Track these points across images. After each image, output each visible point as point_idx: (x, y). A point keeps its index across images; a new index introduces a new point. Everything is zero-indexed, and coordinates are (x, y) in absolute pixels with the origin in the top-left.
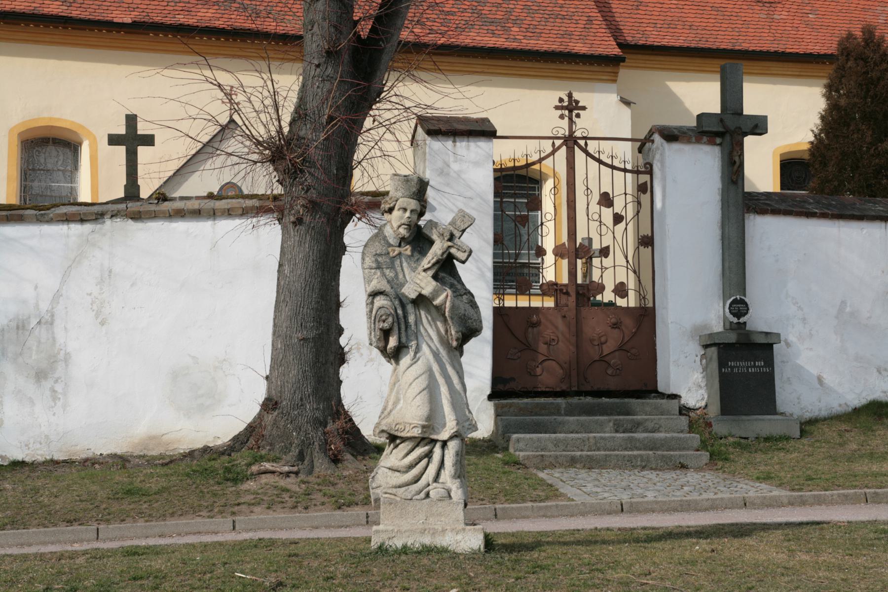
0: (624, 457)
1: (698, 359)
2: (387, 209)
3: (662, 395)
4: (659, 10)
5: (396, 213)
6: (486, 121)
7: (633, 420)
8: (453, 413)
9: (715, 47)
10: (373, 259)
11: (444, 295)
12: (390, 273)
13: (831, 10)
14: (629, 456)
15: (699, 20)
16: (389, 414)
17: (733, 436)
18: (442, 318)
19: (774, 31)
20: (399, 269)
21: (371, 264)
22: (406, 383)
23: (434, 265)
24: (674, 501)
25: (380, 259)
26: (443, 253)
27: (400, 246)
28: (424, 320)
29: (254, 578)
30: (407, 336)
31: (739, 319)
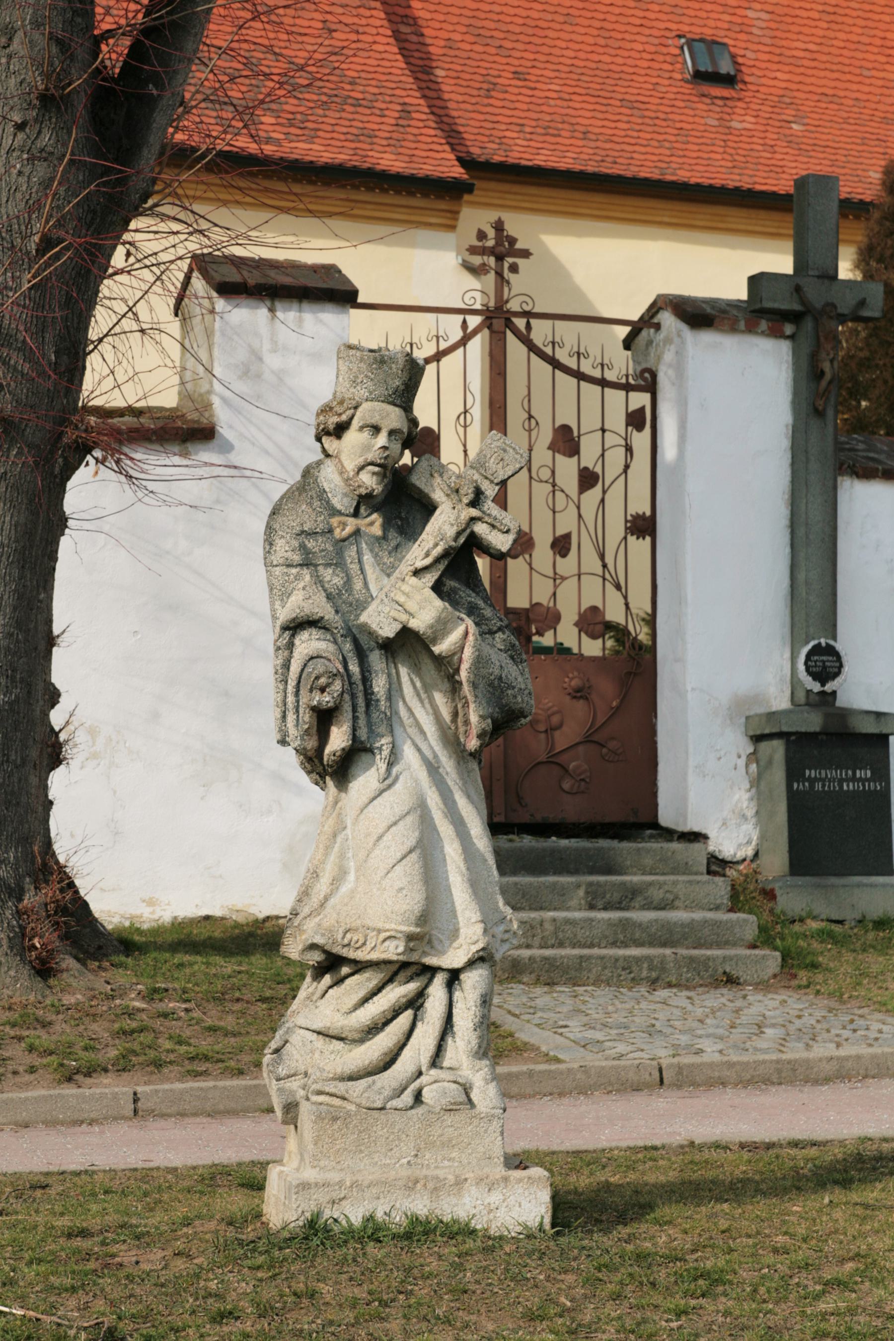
0: (617, 960)
1: (742, 762)
2: (331, 427)
3: (669, 834)
4: (528, 100)
5: (352, 436)
6: (331, 270)
7: (623, 884)
8: (474, 906)
9: (629, 174)
10: (296, 544)
11: (461, 630)
12: (332, 578)
13: (829, 118)
14: (626, 958)
15: (600, 123)
16: (322, 905)
17: (814, 918)
18: (447, 685)
19: (733, 152)
20: (354, 568)
21: (289, 554)
22: (368, 835)
23: (437, 560)
24: (764, 1062)
25: (311, 544)
26: (459, 534)
27: (356, 514)
28: (407, 689)
29: (32, 1313)
30: (370, 725)
31: (823, 685)
